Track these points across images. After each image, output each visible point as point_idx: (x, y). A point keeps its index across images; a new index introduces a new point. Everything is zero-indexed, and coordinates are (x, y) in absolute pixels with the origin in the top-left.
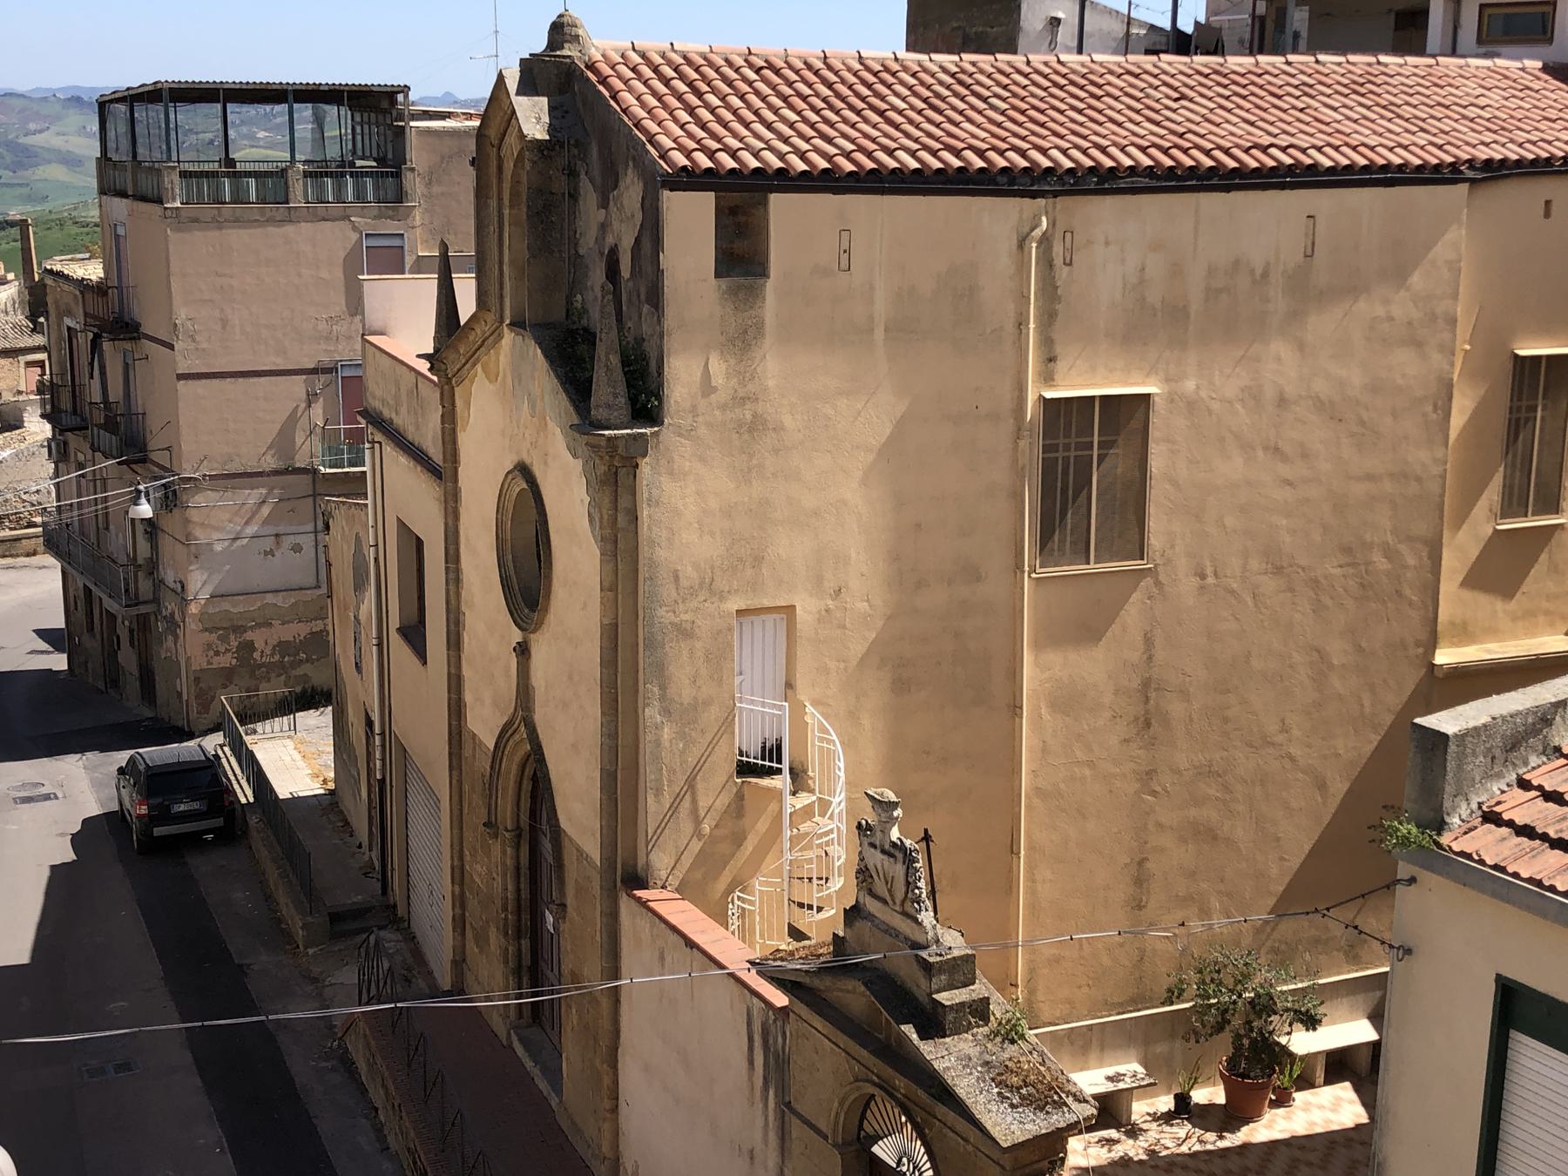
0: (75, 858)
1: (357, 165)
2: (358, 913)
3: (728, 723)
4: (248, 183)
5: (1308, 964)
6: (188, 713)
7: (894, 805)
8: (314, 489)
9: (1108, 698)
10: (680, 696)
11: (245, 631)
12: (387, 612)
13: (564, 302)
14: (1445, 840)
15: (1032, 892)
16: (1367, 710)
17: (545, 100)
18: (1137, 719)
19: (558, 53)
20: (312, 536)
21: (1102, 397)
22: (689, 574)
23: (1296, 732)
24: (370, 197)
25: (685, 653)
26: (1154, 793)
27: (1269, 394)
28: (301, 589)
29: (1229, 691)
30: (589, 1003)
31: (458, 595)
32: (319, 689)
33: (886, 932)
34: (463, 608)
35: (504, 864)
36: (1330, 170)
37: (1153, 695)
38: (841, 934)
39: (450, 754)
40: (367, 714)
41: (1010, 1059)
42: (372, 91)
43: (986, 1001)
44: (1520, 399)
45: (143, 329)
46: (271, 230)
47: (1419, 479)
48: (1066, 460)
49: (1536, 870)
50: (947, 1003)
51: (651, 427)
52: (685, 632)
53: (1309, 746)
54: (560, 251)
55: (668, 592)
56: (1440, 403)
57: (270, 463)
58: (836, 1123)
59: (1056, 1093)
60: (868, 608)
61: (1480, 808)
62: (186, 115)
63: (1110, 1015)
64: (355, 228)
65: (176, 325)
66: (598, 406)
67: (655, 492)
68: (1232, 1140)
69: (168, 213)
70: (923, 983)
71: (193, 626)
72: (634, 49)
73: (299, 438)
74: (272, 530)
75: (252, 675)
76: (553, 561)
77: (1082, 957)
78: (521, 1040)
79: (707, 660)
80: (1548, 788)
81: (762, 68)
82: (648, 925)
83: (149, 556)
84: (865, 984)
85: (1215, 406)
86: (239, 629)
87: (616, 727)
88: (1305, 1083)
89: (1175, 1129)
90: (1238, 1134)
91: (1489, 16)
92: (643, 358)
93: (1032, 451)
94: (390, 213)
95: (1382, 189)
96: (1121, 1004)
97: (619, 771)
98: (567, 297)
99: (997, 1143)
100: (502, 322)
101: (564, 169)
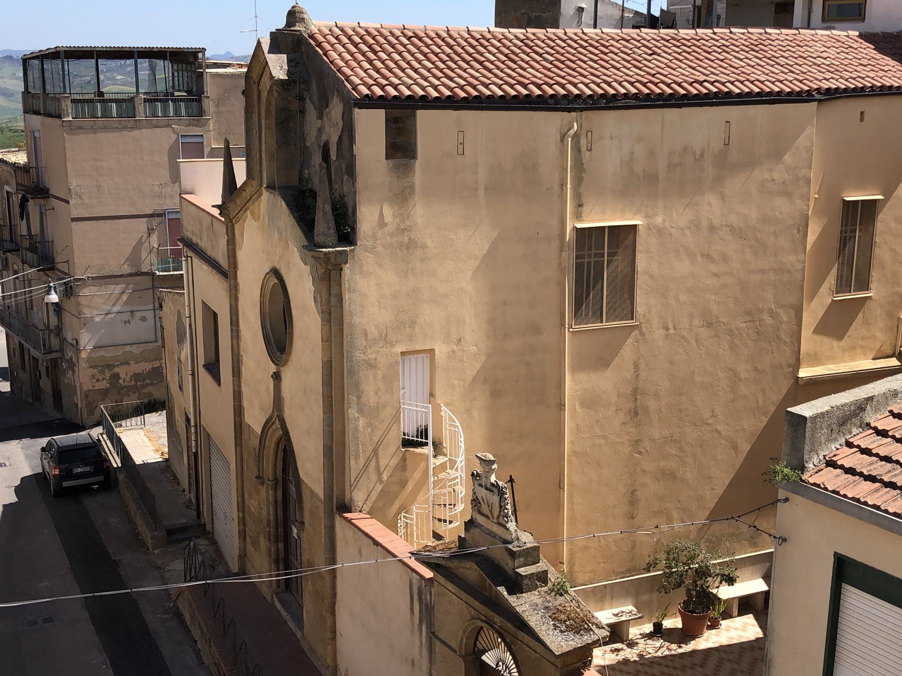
2: (183, 529)
3: (396, 418)
4: (111, 105)
5: (727, 548)
6: (81, 414)
7: (493, 462)
9: (614, 399)
10: (369, 402)
15: (571, 510)
17: (285, 56)
18: (630, 411)
19: (292, 28)
20: (153, 311)
21: (609, 227)
22: (373, 331)
26: (640, 453)
27: (704, 223)
31: (238, 345)
32: (158, 401)
34: (242, 353)
35: (268, 499)
38: (463, 536)
40: (186, 414)
41: (560, 605)
42: (183, 52)
43: (546, 572)
44: (846, 225)
45: (52, 192)
47: (789, 272)
48: (589, 263)
51: (350, 246)
52: (371, 365)
55: (361, 342)
57: (127, 269)
59: (586, 623)
60: (476, 350)
61: (825, 458)
62: (74, 66)
64: (174, 132)
65: (70, 189)
69: (65, 124)
70: (510, 563)
71: (84, 365)
73: (144, 255)
75: (119, 393)
76: (294, 321)
77: (600, 546)
78: (280, 601)
83: (57, 324)
84: (477, 564)
85: (673, 231)
86: (110, 367)
87: (332, 421)
88: (727, 615)
93: (569, 258)
96: (622, 573)
100: (261, 186)
101: (297, 97)
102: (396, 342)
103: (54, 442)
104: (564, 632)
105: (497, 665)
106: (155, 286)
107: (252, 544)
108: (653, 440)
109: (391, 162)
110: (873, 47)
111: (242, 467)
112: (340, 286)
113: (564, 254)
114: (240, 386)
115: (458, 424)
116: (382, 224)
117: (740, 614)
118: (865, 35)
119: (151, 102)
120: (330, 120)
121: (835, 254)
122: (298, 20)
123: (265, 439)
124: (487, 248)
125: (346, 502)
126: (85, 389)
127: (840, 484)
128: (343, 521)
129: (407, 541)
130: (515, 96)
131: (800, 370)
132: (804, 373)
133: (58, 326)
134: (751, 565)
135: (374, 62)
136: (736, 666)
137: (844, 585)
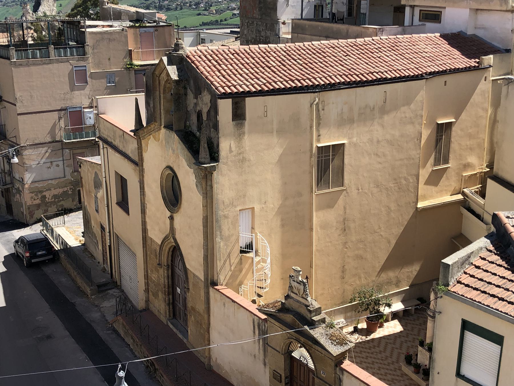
0: (6, 270)
1: (70, 44)
2: (105, 285)
3: (238, 240)
4: (37, 52)
5: (386, 289)
6: (26, 218)
7: (300, 271)
8: (62, 147)
9: (335, 224)
10: (225, 234)
11: (43, 192)
12: (111, 197)
13: (184, 124)
14: (449, 288)
15: (316, 277)
16: (401, 221)
17: (175, 66)
18: (342, 229)
19: (178, 53)
20: (62, 161)
21: (332, 145)
22: (227, 201)
23: (383, 229)
24: (75, 54)
25: (226, 223)
26: (347, 248)
27: (375, 140)
28: (59, 178)
29: (365, 219)
30: (198, 315)
31: (144, 199)
32: (67, 209)
33: (297, 302)
35: (164, 275)
36: (390, 79)
37: (346, 222)
38: (284, 301)
39: (143, 243)
40: (101, 225)
41: (332, 333)
42: (74, 21)
43: (325, 318)
44: (438, 133)
45: (3, 98)
46: (45, 66)
47: (413, 159)
49: (471, 295)
50: (316, 320)
51: (216, 163)
52: (226, 217)
53: (386, 232)
54: (182, 110)
55: (221, 207)
56: (418, 138)
57: (49, 139)
58: (282, 348)
59: (345, 341)
60: (273, 206)
61: (456, 280)
63: (336, 307)
64: (71, 65)
65: (16, 98)
66: (201, 158)
67: (218, 180)
68: (369, 338)
69: (12, 63)
70: (309, 315)
71: (27, 192)
72: (198, 49)
73: (57, 131)
74: (49, 160)
75: (46, 205)
77: (329, 293)
78: (171, 323)
79: (232, 224)
80: (471, 274)
81: (234, 54)
82: (219, 296)
83: (9, 169)
84: (293, 316)
85: (361, 144)
86: (41, 192)
87: (208, 243)
88: (387, 321)
89: (354, 336)
90: (371, 336)
91: (422, 13)
92: (212, 143)
93: (314, 160)
94: (82, 59)
95: (403, 83)
96: (339, 304)
97: (209, 255)
98: (185, 122)
99: (333, 355)
100: (161, 126)
101: (183, 87)
102: (237, 205)
103: (23, 238)
104: (336, 345)
105: (300, 358)
106: (63, 148)
107: (153, 295)
108: (352, 242)
109: (234, 123)
110: (447, 43)
111: (147, 258)
112: (212, 181)
113: (313, 159)
114: (145, 219)
115: (266, 242)
116: (231, 151)
117: (392, 319)
118: (443, 35)
119: (58, 49)
120: (202, 101)
121: (433, 148)
122: (180, 48)
123: (163, 246)
124: (278, 159)
125: (215, 280)
126: (28, 204)
127: (464, 291)
128: (214, 290)
129: (245, 298)
130: (290, 88)
131: (418, 203)
132: (420, 205)
133: (10, 170)
134: (396, 296)
135: (221, 71)
136: (394, 346)
137: (465, 331)
